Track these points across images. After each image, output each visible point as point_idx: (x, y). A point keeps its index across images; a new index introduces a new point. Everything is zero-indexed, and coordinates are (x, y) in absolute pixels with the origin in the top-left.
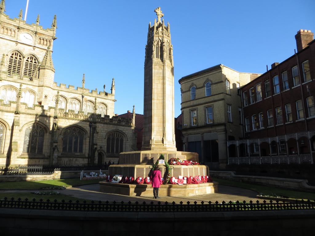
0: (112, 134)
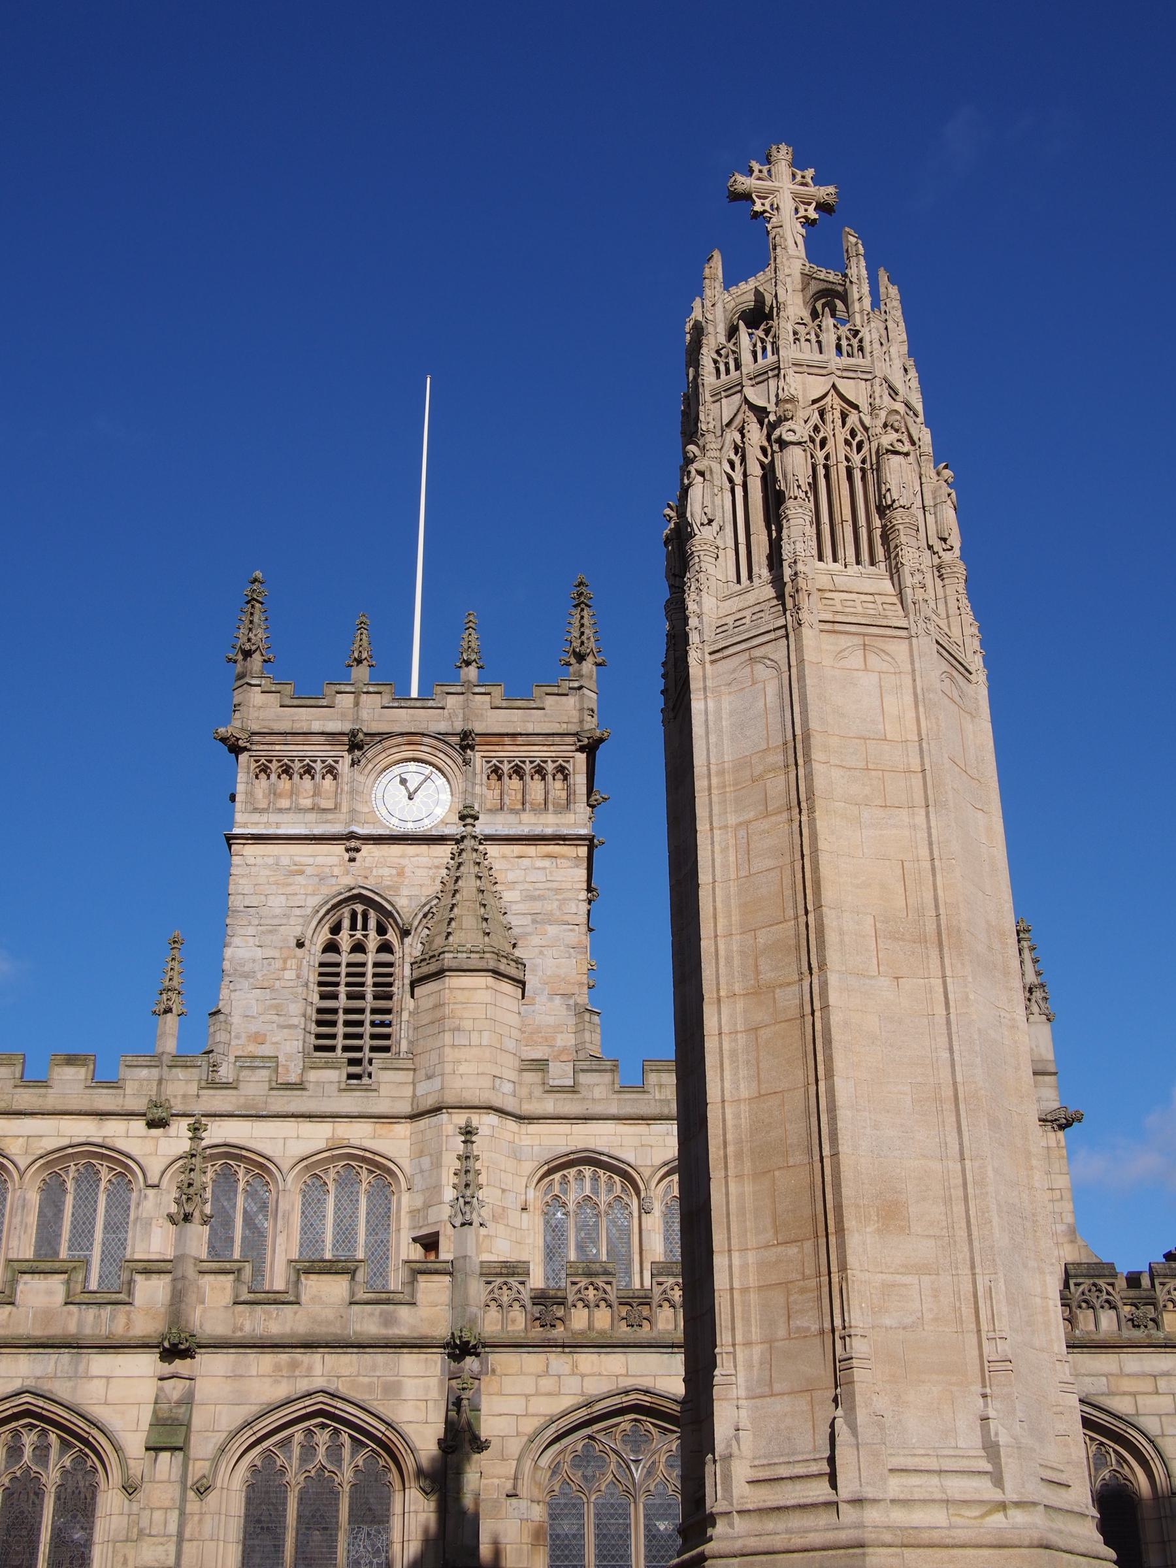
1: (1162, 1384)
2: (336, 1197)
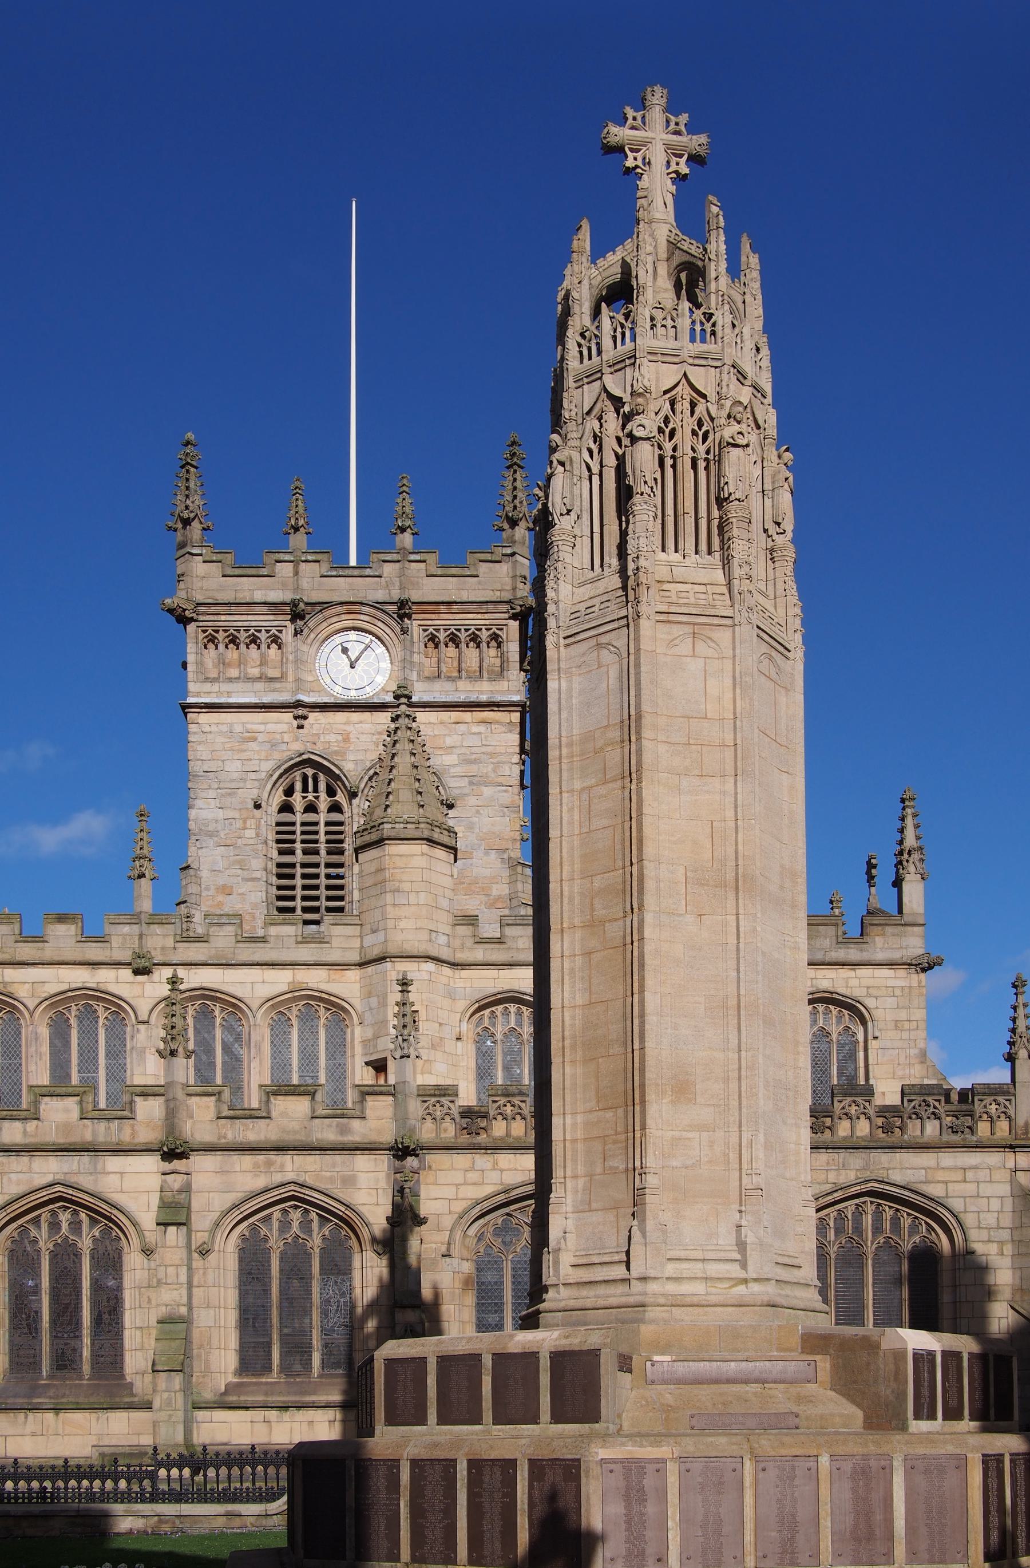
0: (841, 1216)
1: (970, 1175)
2: (299, 1029)
